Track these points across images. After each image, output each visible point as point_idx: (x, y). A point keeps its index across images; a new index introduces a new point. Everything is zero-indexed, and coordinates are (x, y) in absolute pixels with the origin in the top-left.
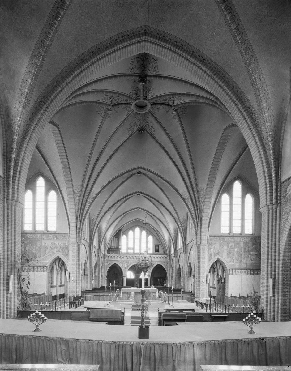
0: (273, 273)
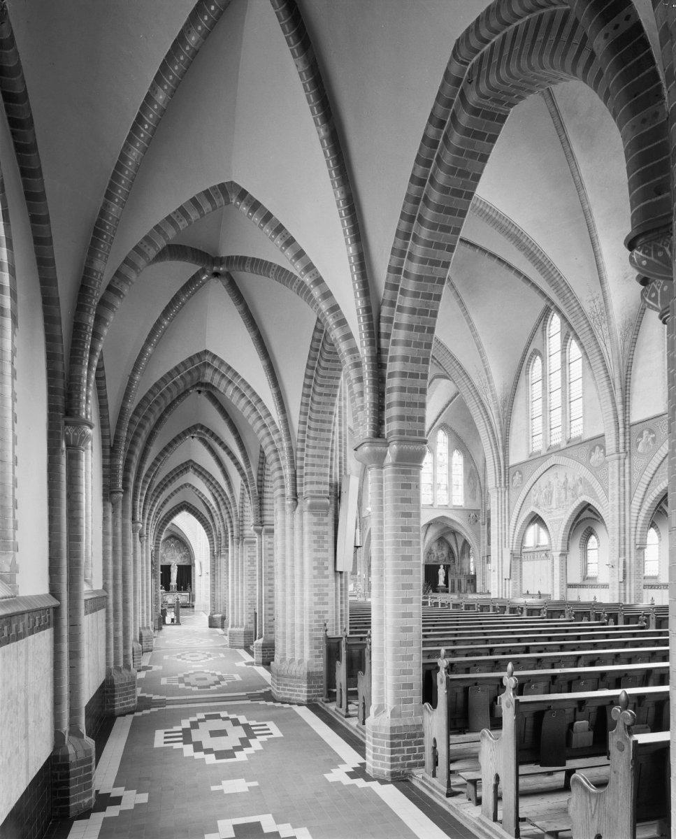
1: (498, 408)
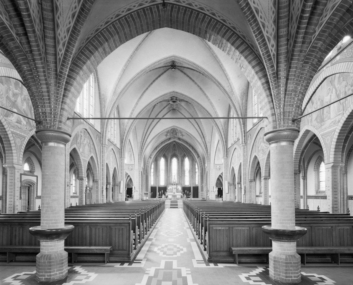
1: (222, 126)
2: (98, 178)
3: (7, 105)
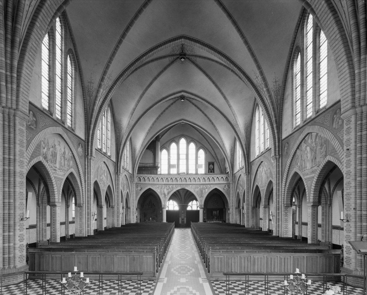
0: (89, 217)
2: (82, 202)
3: (308, 291)
